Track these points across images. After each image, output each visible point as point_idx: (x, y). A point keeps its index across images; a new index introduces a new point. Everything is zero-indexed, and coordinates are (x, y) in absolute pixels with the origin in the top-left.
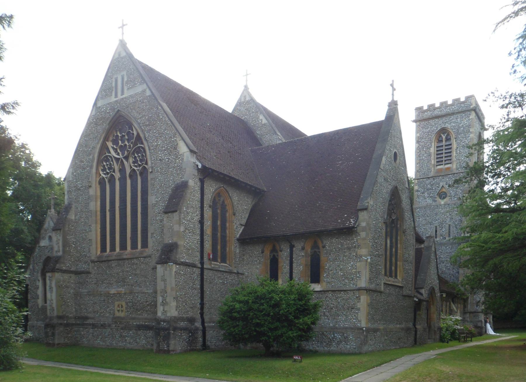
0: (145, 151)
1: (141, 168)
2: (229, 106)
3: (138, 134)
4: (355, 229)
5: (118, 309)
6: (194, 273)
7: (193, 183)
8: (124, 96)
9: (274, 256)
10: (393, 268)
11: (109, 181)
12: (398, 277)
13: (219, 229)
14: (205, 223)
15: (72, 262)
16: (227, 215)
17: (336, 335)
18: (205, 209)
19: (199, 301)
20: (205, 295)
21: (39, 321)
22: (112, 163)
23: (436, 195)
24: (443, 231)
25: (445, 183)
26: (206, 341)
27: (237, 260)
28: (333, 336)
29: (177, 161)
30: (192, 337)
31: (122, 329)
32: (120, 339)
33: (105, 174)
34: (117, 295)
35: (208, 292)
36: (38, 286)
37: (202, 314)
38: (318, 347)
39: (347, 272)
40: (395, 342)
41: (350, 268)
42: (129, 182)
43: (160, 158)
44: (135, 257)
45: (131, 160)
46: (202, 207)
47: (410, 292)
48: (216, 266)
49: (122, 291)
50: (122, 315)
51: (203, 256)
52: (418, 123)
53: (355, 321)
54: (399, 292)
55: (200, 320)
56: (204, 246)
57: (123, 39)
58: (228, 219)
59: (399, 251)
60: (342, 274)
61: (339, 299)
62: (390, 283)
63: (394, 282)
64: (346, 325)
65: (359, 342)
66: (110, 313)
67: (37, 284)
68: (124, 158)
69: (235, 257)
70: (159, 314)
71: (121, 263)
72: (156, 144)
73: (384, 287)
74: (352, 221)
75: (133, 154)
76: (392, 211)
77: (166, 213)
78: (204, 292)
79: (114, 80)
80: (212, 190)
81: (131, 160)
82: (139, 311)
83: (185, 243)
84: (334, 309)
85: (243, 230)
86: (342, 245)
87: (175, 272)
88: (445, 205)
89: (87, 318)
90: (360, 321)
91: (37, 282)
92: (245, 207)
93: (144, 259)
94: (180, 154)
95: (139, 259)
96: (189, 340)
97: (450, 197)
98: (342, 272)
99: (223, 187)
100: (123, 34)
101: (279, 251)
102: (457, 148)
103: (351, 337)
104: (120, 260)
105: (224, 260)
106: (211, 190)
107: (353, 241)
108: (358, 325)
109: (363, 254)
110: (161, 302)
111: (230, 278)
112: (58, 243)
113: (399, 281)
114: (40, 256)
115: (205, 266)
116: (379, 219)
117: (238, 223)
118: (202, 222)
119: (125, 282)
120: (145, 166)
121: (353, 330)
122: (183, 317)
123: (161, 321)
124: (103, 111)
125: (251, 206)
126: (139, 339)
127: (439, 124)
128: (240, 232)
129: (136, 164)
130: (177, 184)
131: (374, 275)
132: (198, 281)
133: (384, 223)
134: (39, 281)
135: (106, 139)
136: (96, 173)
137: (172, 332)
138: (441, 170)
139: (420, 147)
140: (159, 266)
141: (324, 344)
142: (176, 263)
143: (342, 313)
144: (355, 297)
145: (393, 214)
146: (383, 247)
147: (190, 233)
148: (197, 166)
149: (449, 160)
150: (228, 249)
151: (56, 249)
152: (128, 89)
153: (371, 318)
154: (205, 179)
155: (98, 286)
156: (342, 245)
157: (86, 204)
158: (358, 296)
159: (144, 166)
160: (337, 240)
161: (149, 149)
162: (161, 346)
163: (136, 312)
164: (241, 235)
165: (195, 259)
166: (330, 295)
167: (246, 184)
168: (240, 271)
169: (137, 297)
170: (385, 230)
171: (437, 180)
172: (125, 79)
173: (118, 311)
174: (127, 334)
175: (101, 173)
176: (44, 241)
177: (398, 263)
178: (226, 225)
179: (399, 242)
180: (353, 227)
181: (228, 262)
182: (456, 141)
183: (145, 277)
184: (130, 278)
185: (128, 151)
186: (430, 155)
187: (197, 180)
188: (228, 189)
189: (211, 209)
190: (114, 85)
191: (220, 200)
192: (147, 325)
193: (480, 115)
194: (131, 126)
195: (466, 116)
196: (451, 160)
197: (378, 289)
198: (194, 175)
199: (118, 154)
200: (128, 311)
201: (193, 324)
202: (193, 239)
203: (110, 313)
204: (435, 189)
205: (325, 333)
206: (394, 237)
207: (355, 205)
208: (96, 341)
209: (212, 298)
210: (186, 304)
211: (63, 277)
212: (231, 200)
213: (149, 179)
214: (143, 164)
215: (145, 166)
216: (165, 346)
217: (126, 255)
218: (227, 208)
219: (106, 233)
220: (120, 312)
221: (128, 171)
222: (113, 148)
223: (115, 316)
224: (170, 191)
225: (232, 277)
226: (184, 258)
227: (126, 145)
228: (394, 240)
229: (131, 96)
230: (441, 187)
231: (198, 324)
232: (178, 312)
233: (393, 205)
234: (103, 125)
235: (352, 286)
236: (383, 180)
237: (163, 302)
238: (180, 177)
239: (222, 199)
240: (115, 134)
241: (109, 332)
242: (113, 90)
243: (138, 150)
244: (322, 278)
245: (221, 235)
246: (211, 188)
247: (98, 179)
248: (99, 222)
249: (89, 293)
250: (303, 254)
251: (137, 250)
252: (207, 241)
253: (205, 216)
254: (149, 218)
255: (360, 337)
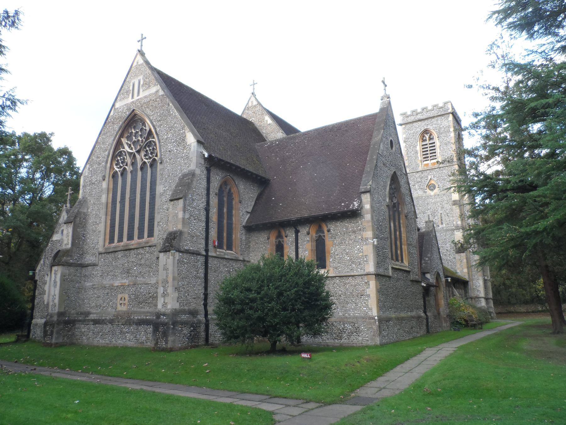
0: (155, 145)
1: (151, 160)
2: (237, 109)
3: (150, 130)
4: (360, 211)
5: (121, 302)
6: (198, 261)
7: (201, 172)
8: (139, 97)
9: (280, 241)
10: (399, 252)
11: (122, 174)
12: (404, 261)
13: (225, 216)
14: (211, 210)
15: (80, 255)
16: (234, 202)
17: (346, 325)
18: (211, 197)
19: (203, 291)
20: (209, 284)
21: (43, 319)
22: (125, 157)
23: (425, 187)
24: (436, 220)
25: (433, 176)
26: (209, 335)
27: (244, 247)
28: (343, 326)
29: (185, 151)
30: (194, 332)
31: (122, 324)
32: (120, 336)
33: (118, 168)
34: (120, 287)
35: (212, 281)
36: (46, 281)
37: (205, 305)
38: (328, 339)
39: (353, 256)
40: (408, 332)
41: (356, 252)
42: (139, 173)
43: (169, 149)
44: (140, 246)
45: (143, 153)
46: (208, 194)
47: (417, 277)
48: (222, 254)
49: (126, 283)
50: (124, 308)
51: (208, 244)
52: (404, 126)
53: (365, 309)
54: (407, 277)
55: (203, 312)
56: (210, 233)
57: (141, 50)
58: (234, 207)
59: (402, 235)
60: (348, 258)
61: (348, 285)
62: (397, 267)
63: (401, 266)
64: (357, 313)
65: (372, 334)
66: (113, 307)
67: (46, 279)
68: (136, 152)
69: (242, 244)
70: (160, 306)
71: (127, 253)
72: (166, 137)
73: (392, 272)
74: (356, 204)
75: (145, 147)
76: (393, 195)
77: (171, 200)
78: (209, 281)
79: (132, 84)
80: (219, 178)
81: (143, 153)
82: (141, 304)
83: (189, 230)
84: (343, 297)
85: (249, 217)
86: (347, 229)
87: (178, 260)
88: (435, 195)
89: (89, 313)
90: (371, 309)
91: (46, 276)
92: (251, 195)
93: (149, 248)
94: (188, 145)
95: (145, 248)
96: (191, 334)
97: (439, 188)
98: (348, 257)
99: (229, 175)
100: (142, 45)
101: (284, 237)
102: (440, 145)
103: (362, 328)
104: (126, 250)
105: (230, 247)
106: (218, 178)
107: (358, 224)
108: (369, 314)
109: (369, 237)
110: (162, 293)
111: (236, 265)
112: (68, 236)
113: (406, 264)
114: (52, 250)
115: (210, 254)
116: (382, 202)
117: (244, 210)
118: (207, 210)
119: (130, 273)
120: (155, 157)
121: (364, 320)
122: (185, 310)
123: (161, 315)
124: (121, 111)
125: (257, 194)
126: (139, 335)
127: (421, 127)
128: (246, 219)
129: (147, 157)
130: (184, 172)
131: (380, 261)
132: (202, 270)
133: (387, 206)
134: (48, 275)
135: (121, 136)
136: (111, 167)
137: (172, 327)
138: (427, 165)
139: (407, 146)
140: (161, 255)
141: (334, 336)
142: (180, 251)
143: (352, 300)
144: (364, 283)
145: (394, 198)
146: (388, 230)
147: (195, 220)
148: (204, 155)
149: (434, 157)
150: (234, 236)
151: (65, 242)
152: (143, 91)
153: (381, 306)
154: (211, 168)
155: (103, 278)
156: (347, 229)
157: (99, 196)
158: (366, 281)
159: (154, 158)
160: (341, 223)
161: (159, 142)
162: (159, 343)
163: (138, 305)
164: (247, 222)
165: (200, 246)
166: (338, 281)
167: (252, 173)
168: (246, 259)
169: (140, 288)
170: (388, 213)
171: (425, 174)
172: (142, 83)
173: (121, 304)
174: (127, 330)
175: (115, 167)
176: (57, 235)
177: (403, 246)
178: (232, 212)
179: (402, 225)
180: (357, 210)
181: (234, 249)
182: (438, 140)
183: (149, 267)
184: (135, 268)
185: (140, 145)
186: (417, 152)
187: (204, 168)
188: (235, 178)
189: (217, 197)
190: (131, 88)
191: (226, 188)
192: (148, 319)
193: (457, 118)
194: (144, 124)
195: (445, 119)
196: (436, 156)
197: (387, 274)
198: (200, 163)
199: (132, 149)
200: (130, 305)
201: (196, 317)
202: (198, 226)
203: (113, 307)
204: (425, 181)
205: (334, 323)
206: (397, 221)
207: (357, 188)
208: (96, 339)
209: (217, 287)
210: (188, 295)
211: (69, 270)
212: (238, 188)
213: (158, 170)
214: (153, 156)
215: (155, 157)
216: (164, 343)
217: (133, 245)
218: (234, 196)
219: (115, 224)
220: (123, 306)
221: (139, 164)
222: (127, 144)
223: (117, 310)
224: (177, 179)
225: (238, 265)
226: (188, 245)
227: (138, 140)
228: (397, 223)
229: (145, 97)
230: (429, 179)
231: (201, 317)
232: (180, 304)
233: (393, 189)
234: (119, 123)
235: (362, 272)
236: (382, 165)
237: (164, 293)
238: (187, 166)
239: (228, 187)
240: (130, 131)
241: (110, 328)
242: (130, 93)
243: (149, 144)
244: (328, 263)
245: (227, 223)
246: (217, 179)
247: (112, 173)
248: (109, 213)
249: (94, 286)
250: (308, 239)
251: (143, 240)
252: (212, 227)
253: (211, 203)
254: (156, 207)
255: (372, 328)
